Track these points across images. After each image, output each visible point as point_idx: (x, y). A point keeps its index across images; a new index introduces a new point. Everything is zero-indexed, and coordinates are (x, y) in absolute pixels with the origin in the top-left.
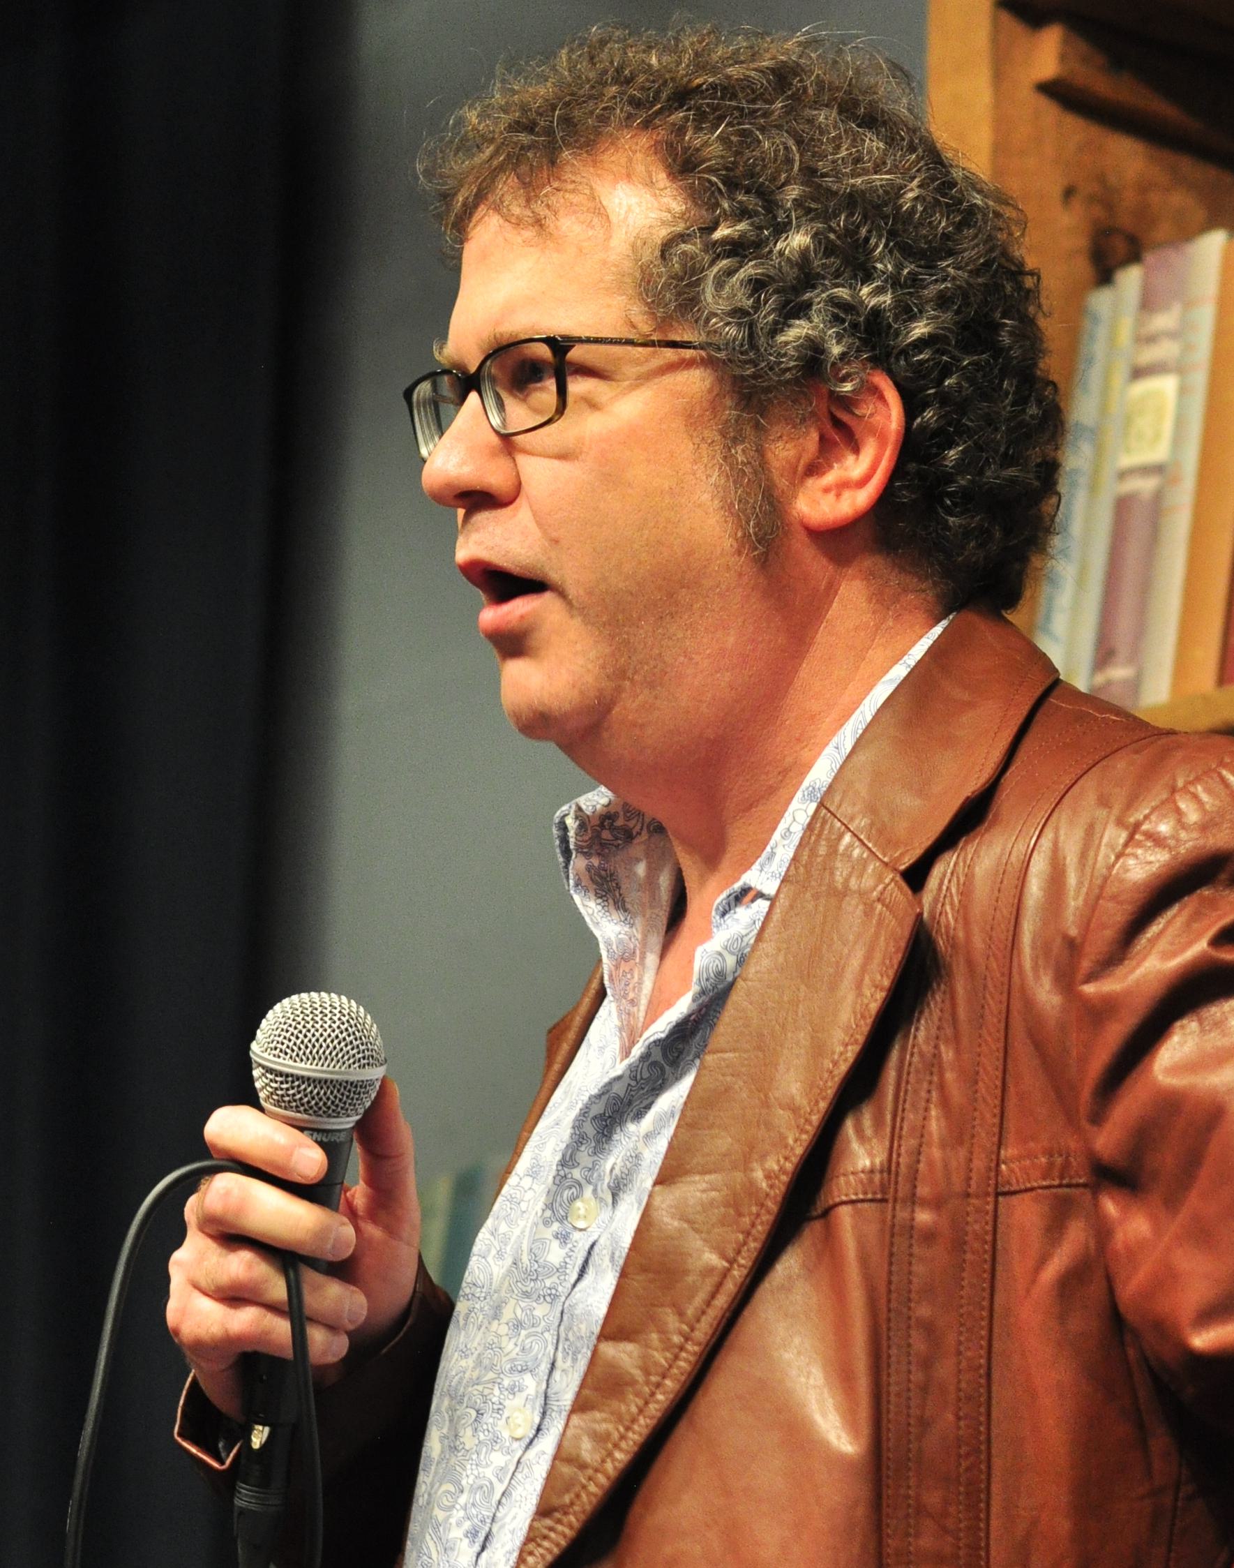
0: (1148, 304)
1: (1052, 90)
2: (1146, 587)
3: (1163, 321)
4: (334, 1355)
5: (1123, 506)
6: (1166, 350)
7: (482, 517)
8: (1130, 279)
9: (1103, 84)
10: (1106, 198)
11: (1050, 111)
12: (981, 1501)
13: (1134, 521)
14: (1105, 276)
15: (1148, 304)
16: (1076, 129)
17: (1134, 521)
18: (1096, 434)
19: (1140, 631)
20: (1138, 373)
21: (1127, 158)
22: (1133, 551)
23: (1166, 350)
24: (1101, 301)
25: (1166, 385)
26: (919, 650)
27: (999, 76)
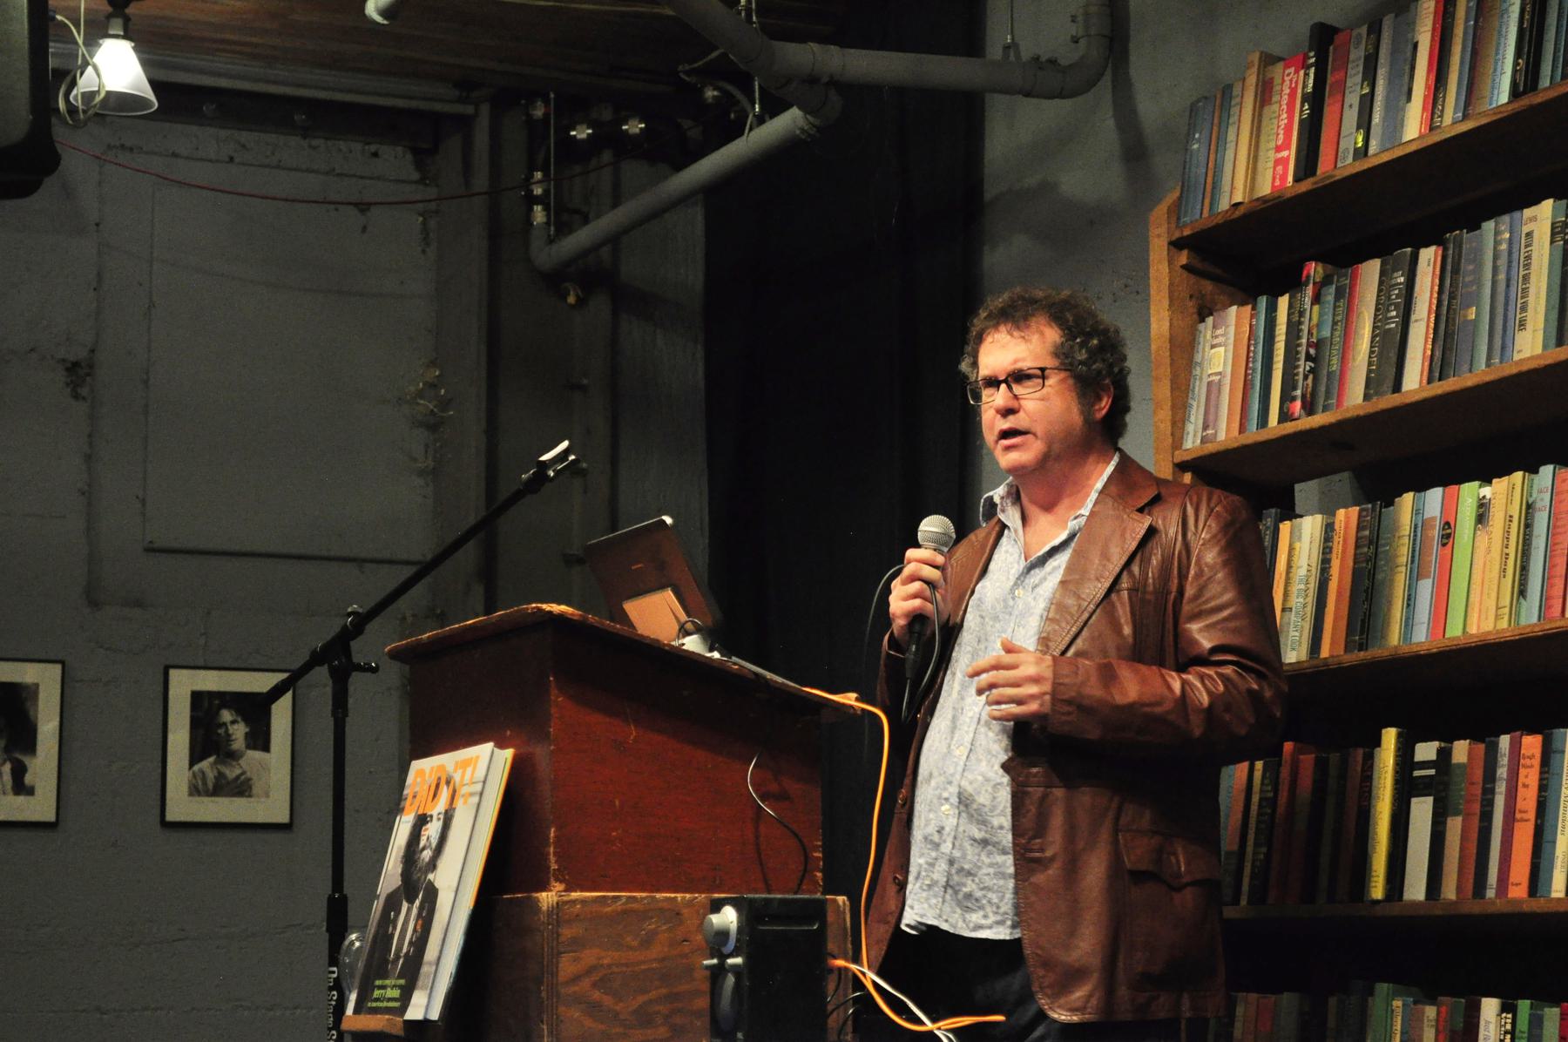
0: (1215, 327)
1: (1183, 267)
2: (1217, 407)
3: (1219, 332)
4: (1042, 334)
5: (1210, 384)
6: (1221, 340)
7: (1023, 564)
8: (1210, 320)
9: (1198, 264)
10: (1202, 297)
11: (1185, 274)
12: (532, 200)
13: (1213, 389)
14: (1202, 320)
15: (1215, 327)
16: (1193, 279)
17: (1213, 389)
18: (1200, 364)
19: (1216, 420)
20: (1213, 347)
21: (1208, 286)
22: (1213, 397)
23: (1221, 340)
24: (1201, 326)
25: (1222, 349)
26: (1110, 468)
27: (1170, 262)
